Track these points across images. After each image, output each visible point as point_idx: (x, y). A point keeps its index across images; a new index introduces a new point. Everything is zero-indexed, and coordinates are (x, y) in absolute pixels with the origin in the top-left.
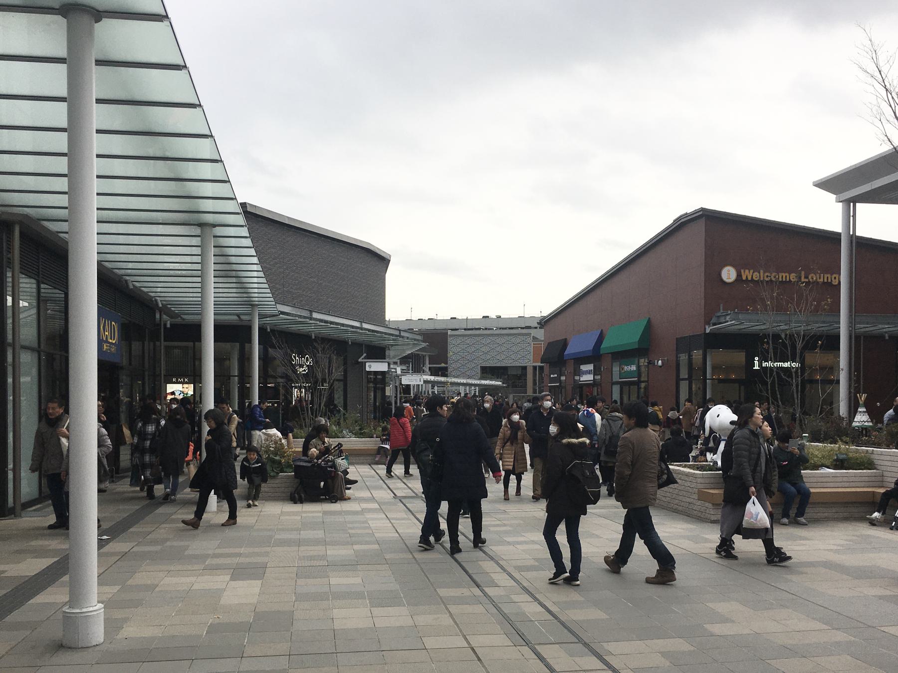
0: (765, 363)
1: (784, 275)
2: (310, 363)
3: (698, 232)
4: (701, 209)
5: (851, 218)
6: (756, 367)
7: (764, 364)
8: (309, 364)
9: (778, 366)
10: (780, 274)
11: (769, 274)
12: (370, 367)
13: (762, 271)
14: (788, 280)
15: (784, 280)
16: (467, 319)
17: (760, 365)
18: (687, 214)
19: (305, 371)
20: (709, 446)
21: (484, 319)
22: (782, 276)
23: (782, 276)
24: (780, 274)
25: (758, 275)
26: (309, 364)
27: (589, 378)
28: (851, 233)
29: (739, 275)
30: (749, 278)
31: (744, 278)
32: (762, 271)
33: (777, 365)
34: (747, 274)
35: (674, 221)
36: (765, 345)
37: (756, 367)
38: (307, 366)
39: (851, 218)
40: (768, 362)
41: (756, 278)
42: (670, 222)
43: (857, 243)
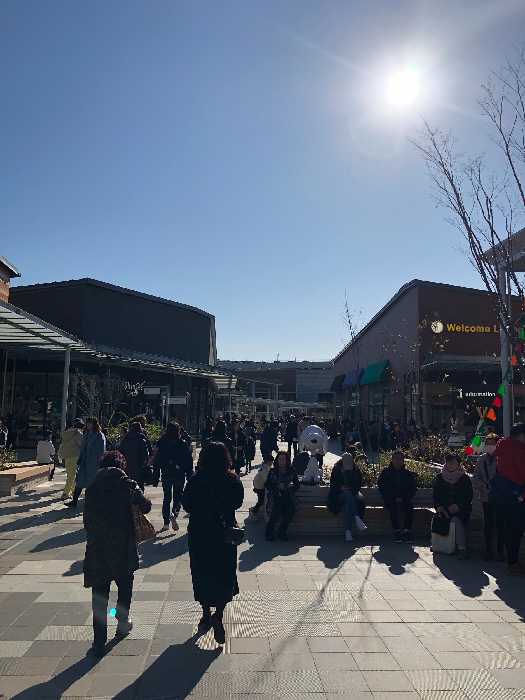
0: (468, 393)
1: (480, 328)
2: (140, 388)
3: (414, 295)
4: (414, 281)
5: (507, 282)
6: (461, 396)
7: (467, 394)
8: (139, 389)
9: (480, 395)
10: (477, 327)
11: (468, 327)
12: (147, 391)
13: (463, 326)
14: (483, 331)
15: (480, 331)
16: (313, 362)
17: (464, 394)
18: (407, 284)
19: (135, 394)
20: (338, 458)
21: (304, 362)
22: (479, 329)
23: (479, 329)
24: (477, 327)
25: (460, 328)
26: (139, 389)
27: (355, 403)
28: (507, 293)
29: (445, 328)
30: (453, 330)
31: (449, 329)
32: (463, 326)
33: (479, 394)
34: (451, 327)
35: (400, 290)
36: (393, 376)
37: (461, 396)
38: (138, 390)
39: (507, 282)
40: (470, 393)
41: (458, 330)
42: (397, 291)
43: (512, 300)
